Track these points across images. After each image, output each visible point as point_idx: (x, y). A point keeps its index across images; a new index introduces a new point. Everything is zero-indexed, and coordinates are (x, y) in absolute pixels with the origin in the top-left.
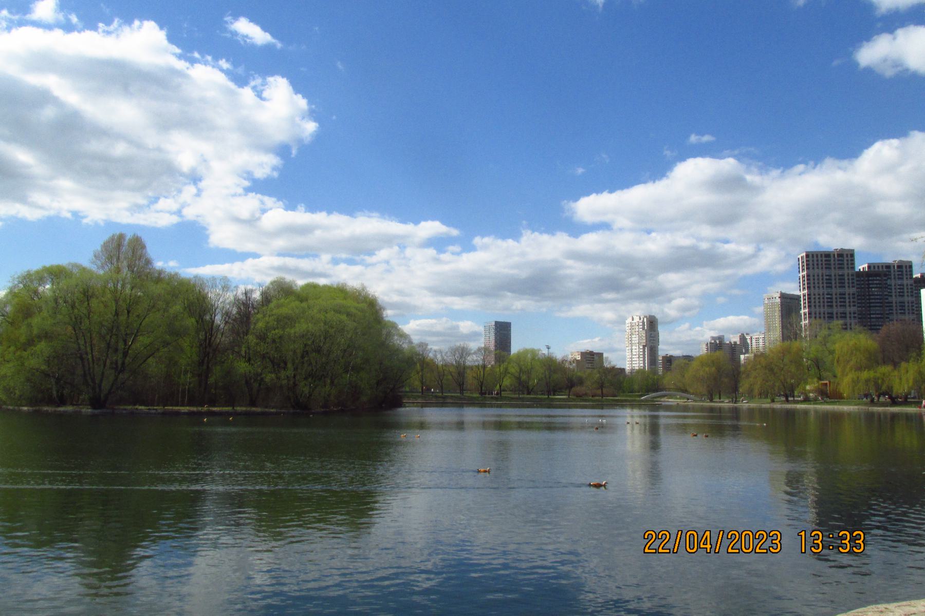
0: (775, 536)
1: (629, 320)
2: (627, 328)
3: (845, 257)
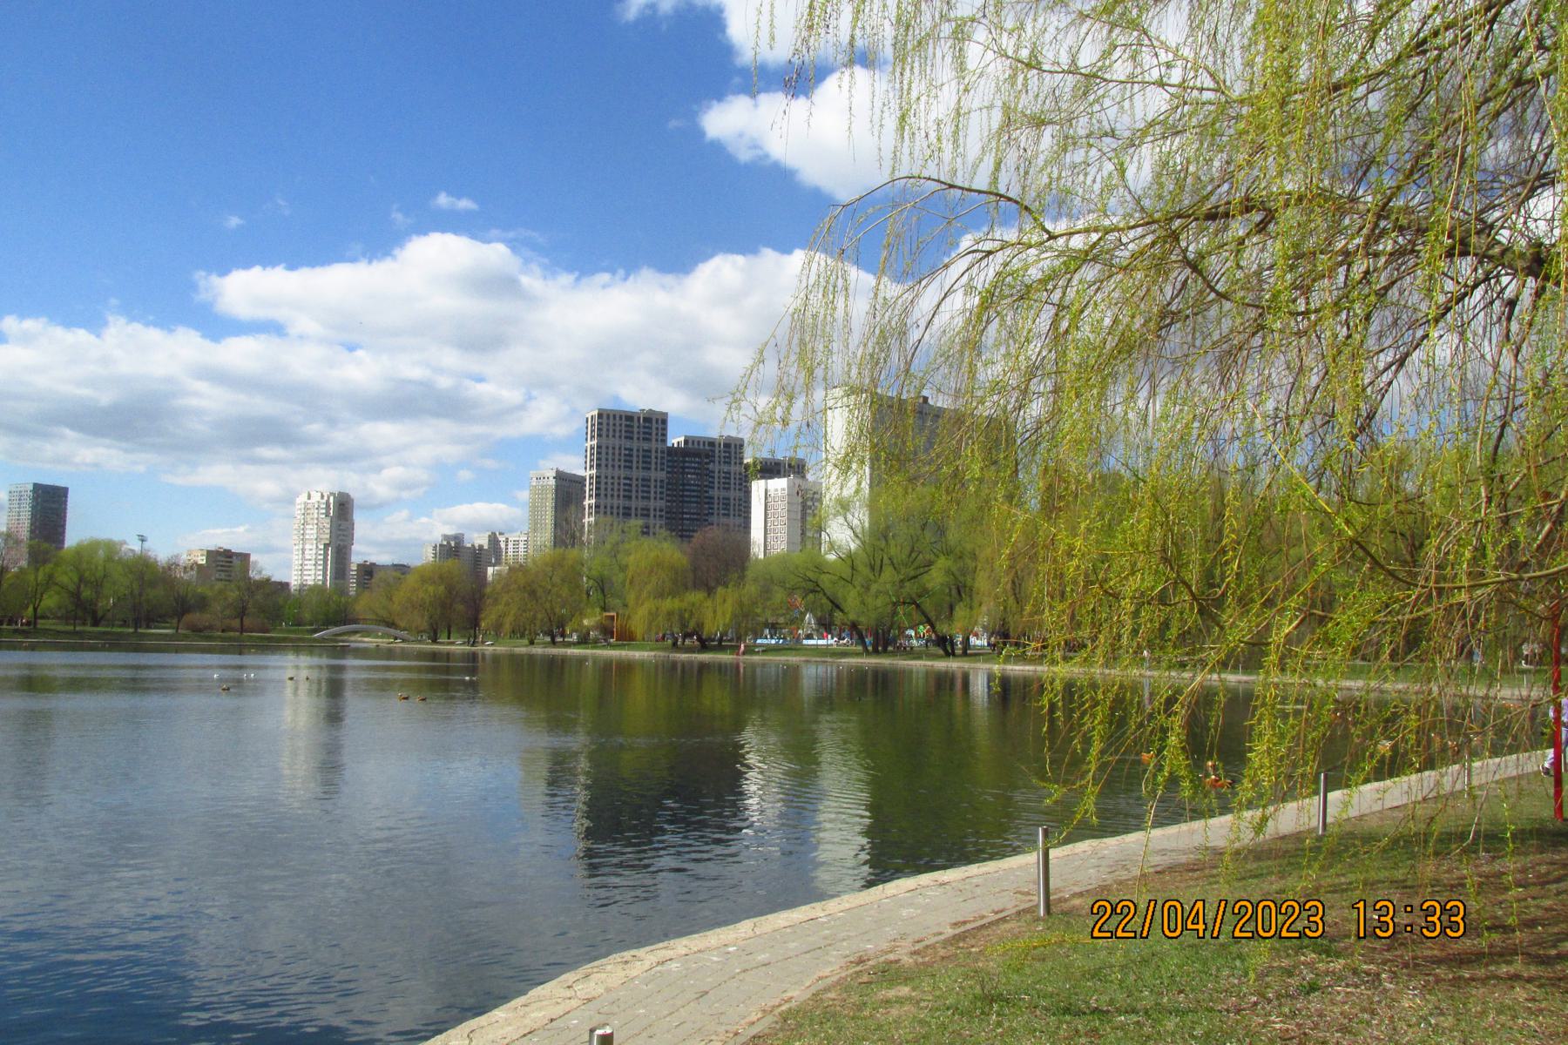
0: (1313, 909)
1: (303, 498)
2: (298, 513)
3: (654, 423)
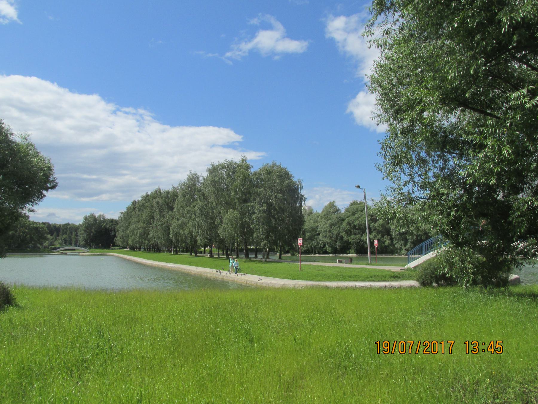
0: (475, 344)
